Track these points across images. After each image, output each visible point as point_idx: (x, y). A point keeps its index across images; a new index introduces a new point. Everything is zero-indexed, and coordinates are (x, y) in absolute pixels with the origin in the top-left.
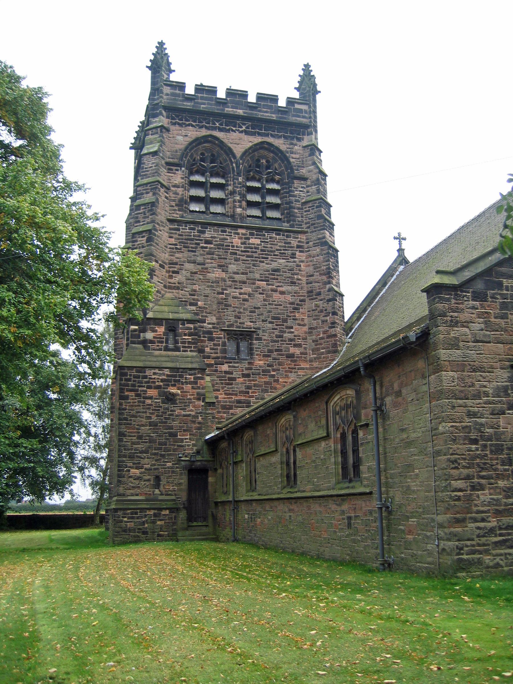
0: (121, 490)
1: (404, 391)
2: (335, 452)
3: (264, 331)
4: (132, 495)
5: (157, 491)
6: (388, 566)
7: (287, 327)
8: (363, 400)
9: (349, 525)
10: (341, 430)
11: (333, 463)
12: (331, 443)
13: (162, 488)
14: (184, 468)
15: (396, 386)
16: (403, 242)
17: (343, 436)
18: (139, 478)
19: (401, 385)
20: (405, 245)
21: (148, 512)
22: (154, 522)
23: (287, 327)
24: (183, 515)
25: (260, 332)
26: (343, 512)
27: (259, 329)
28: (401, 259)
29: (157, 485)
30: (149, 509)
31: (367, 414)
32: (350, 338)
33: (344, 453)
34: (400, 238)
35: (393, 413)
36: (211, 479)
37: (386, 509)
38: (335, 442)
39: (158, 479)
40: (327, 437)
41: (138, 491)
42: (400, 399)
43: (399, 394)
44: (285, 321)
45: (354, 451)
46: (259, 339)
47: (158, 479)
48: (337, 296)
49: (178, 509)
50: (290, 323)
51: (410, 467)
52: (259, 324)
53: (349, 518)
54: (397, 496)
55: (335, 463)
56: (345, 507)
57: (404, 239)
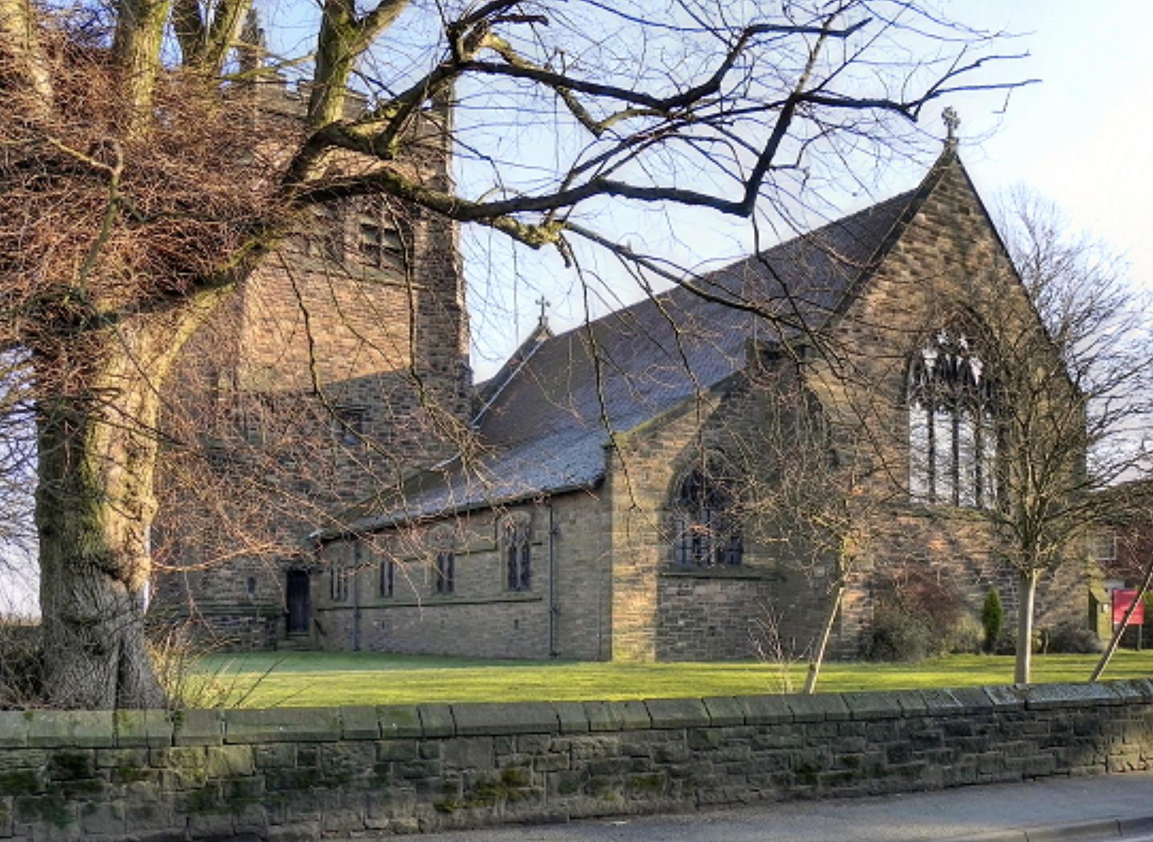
0: (209, 593)
1: (578, 521)
2: (503, 562)
3: (376, 410)
4: (222, 599)
5: (251, 596)
6: (554, 655)
7: (403, 407)
8: (537, 522)
9: (516, 627)
10: (510, 545)
11: (501, 573)
12: (499, 555)
13: (257, 592)
14: (284, 570)
15: (571, 516)
16: (546, 308)
17: (513, 551)
18: (229, 580)
19: (576, 515)
20: (548, 311)
21: (241, 619)
22: (248, 630)
23: (403, 407)
24: (281, 624)
25: (371, 411)
26: (510, 616)
27: (370, 407)
28: (542, 328)
29: (251, 589)
30: (244, 615)
31: (542, 533)
32: (477, 423)
33: (512, 565)
34: (544, 304)
35: (566, 536)
36: (313, 583)
37: (555, 611)
38: (503, 554)
39: (252, 581)
40: (496, 549)
41: (230, 595)
42: (574, 527)
43: (573, 522)
44: (401, 399)
45: (523, 564)
46: (369, 420)
47: (252, 581)
48: (466, 371)
49: (276, 617)
50: (407, 401)
51: (578, 580)
52: (371, 401)
53: (516, 622)
54: (566, 602)
55: (503, 574)
56: (513, 611)
57: (548, 304)
